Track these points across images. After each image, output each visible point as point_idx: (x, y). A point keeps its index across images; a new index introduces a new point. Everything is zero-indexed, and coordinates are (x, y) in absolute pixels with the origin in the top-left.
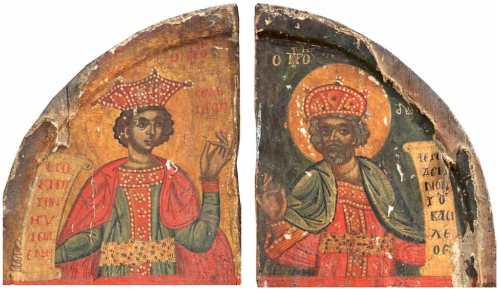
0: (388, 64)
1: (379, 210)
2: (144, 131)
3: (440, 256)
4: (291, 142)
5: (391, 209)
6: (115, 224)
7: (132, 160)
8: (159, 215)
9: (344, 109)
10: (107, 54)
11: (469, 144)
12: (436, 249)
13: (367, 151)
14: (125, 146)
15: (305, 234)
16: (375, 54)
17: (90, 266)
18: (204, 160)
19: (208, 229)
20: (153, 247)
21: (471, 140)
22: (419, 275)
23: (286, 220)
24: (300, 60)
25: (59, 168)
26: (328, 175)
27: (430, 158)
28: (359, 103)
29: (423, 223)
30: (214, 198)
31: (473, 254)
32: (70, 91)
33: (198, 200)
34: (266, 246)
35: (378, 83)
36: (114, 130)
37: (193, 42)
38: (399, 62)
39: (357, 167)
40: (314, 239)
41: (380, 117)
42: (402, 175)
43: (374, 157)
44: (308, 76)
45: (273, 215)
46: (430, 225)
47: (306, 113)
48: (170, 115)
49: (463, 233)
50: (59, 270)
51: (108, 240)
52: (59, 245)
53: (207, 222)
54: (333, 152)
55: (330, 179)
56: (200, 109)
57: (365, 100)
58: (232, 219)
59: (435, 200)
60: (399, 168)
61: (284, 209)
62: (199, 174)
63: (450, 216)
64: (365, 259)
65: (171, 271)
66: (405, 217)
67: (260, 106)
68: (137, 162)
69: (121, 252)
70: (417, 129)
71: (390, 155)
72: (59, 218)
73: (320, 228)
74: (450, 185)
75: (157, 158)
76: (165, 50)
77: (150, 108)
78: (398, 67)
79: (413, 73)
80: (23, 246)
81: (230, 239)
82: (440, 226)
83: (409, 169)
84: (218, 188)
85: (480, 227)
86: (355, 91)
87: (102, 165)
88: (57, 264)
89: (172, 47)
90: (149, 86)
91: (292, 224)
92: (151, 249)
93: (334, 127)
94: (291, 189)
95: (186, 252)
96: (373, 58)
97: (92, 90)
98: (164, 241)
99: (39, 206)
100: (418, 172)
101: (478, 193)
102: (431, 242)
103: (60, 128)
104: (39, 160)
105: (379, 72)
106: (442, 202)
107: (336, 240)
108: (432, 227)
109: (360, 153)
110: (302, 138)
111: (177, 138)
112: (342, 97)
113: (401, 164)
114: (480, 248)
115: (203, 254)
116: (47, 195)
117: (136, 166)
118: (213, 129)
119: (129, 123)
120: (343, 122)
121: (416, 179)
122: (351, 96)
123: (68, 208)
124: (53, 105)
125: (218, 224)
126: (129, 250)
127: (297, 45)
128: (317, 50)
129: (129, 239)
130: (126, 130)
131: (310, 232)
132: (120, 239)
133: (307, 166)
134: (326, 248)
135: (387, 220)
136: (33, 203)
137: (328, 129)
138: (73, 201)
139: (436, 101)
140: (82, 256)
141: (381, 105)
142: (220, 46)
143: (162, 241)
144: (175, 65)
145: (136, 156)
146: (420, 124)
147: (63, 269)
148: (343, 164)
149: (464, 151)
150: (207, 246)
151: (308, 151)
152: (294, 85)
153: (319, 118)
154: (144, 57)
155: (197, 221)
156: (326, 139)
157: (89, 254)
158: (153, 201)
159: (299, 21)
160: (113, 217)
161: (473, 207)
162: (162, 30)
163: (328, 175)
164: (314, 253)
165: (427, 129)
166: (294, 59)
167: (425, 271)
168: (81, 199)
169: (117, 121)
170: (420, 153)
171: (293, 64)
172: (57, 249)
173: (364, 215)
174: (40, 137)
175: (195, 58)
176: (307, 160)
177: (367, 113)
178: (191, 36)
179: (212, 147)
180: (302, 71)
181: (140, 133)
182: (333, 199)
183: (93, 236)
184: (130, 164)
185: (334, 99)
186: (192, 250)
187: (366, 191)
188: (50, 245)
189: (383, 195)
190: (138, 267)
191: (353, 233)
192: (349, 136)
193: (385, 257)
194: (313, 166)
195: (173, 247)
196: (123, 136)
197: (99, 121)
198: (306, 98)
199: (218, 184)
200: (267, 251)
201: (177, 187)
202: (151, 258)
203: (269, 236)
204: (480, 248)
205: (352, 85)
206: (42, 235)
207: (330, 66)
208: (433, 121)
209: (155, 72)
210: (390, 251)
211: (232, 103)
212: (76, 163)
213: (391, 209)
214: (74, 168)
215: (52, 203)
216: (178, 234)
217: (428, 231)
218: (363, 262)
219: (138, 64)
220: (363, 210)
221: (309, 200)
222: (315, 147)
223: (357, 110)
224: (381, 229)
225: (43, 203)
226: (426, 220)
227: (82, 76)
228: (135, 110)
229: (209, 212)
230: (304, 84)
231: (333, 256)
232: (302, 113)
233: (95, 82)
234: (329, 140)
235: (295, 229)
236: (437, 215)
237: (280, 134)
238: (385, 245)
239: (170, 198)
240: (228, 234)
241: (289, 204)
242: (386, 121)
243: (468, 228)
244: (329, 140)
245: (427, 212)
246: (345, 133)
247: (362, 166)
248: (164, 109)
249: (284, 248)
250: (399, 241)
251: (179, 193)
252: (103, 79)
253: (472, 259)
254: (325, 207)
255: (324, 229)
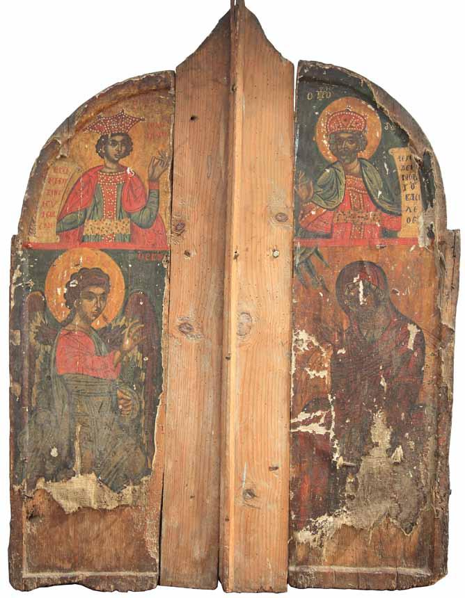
0: (381, 96)
1: (372, 193)
2: (114, 149)
3: (411, 224)
4: (317, 149)
5: (380, 193)
6: (94, 209)
7: (106, 167)
8: (121, 204)
9: (351, 127)
10: (94, 98)
11: (431, 148)
12: (409, 220)
13: (365, 154)
14: (102, 157)
15: (324, 210)
16: (373, 90)
17: (77, 235)
18: (151, 169)
19: (151, 214)
20: (117, 224)
21: (432, 146)
22: (397, 237)
23: (312, 202)
24: (325, 96)
25: (62, 170)
26: (340, 171)
27: (405, 159)
28: (361, 122)
29: (401, 203)
30: (156, 193)
31: (432, 223)
32: (69, 122)
33: (146, 195)
34: (299, 219)
35: (373, 109)
36: (96, 146)
37: (147, 92)
38: (388, 95)
39: (359, 165)
40: (330, 214)
41: (374, 131)
42: (387, 170)
43: (370, 159)
44: (329, 106)
45: (304, 198)
46: (405, 203)
47: (327, 130)
48: (131, 139)
49: (426, 209)
50: (58, 237)
51: (89, 219)
52: (59, 220)
53: (150, 209)
54: (344, 155)
55: (341, 174)
56: (150, 136)
57: (365, 121)
58: (166, 208)
59: (408, 187)
60: (386, 165)
61: (311, 195)
62: (147, 178)
63: (418, 198)
64: (363, 227)
65: (127, 240)
66: (389, 199)
67: (298, 127)
68: (109, 168)
69: (96, 226)
70: (397, 140)
71: (380, 157)
72: (59, 203)
73: (334, 207)
74: (418, 177)
75: (122, 166)
76: (130, 97)
77: (118, 134)
78: (387, 97)
79: (396, 102)
80: (37, 221)
81: (164, 220)
82: (411, 204)
83: (392, 166)
84: (159, 187)
85: (437, 204)
86: (359, 115)
87: (88, 169)
88: (58, 233)
89: (133, 96)
90: (118, 120)
91: (317, 205)
92: (115, 225)
93: (344, 139)
94: (316, 181)
95: (137, 228)
96: (371, 92)
97: (83, 120)
98: (124, 220)
99: (48, 194)
100: (398, 168)
101: (436, 181)
102: (405, 215)
103: (63, 146)
104: (49, 165)
105: (375, 102)
106: (413, 187)
107: (344, 215)
108: (406, 205)
109: (361, 155)
110: (324, 148)
111: (135, 154)
112: (350, 119)
113: (387, 163)
114: (437, 218)
115: (147, 230)
116: (53, 188)
117: (108, 171)
118: (157, 149)
119: (106, 143)
120: (351, 135)
121: (397, 172)
122: (356, 118)
123: (66, 197)
124: (59, 130)
125: (158, 211)
126: (102, 225)
127: (323, 86)
128: (335, 89)
129: (102, 218)
130: (103, 147)
131: (327, 209)
132: (97, 218)
133: (327, 165)
134: (338, 220)
135: (377, 201)
136: (45, 193)
137: (340, 140)
138: (69, 192)
139: (411, 120)
140: (73, 228)
141: (375, 124)
142: (163, 96)
143: (122, 221)
144: (135, 107)
145: (109, 165)
146: (400, 136)
147: (60, 236)
148: (350, 163)
149: (428, 153)
150: (150, 224)
151: (328, 155)
152: (320, 112)
153: (335, 133)
154: (116, 101)
155: (145, 208)
156: (339, 147)
157: (77, 227)
158: (117, 194)
159: (326, 70)
160: (93, 203)
161: (432, 190)
162: (129, 83)
163: (340, 171)
164: (330, 223)
165: (404, 138)
166: (321, 95)
167: (401, 235)
168: (73, 192)
169: (98, 141)
170: (400, 155)
171: (320, 98)
172: (57, 223)
173: (363, 198)
174: (50, 149)
175: (148, 103)
176: (327, 161)
177: (366, 129)
178: (145, 88)
179: (156, 161)
180: (326, 103)
181: (112, 150)
182: (343, 187)
183: (80, 215)
184: (105, 170)
185: (345, 120)
186: (141, 226)
187: (364, 181)
188: (53, 220)
189: (375, 183)
190: (106, 237)
191: (355, 209)
192: (354, 145)
193: (376, 225)
194: (330, 166)
195: (129, 225)
196: (101, 152)
197: (87, 141)
198: (328, 120)
199: (159, 184)
200: (300, 222)
201: (133, 185)
202: (115, 231)
203: (302, 212)
204: (437, 218)
205: (357, 111)
206: (49, 214)
207: (344, 99)
208: (408, 133)
209: (123, 111)
210: (379, 221)
211: (169, 133)
212: (73, 168)
213: (380, 193)
214: (70, 170)
215: (56, 192)
216: (133, 216)
217: (404, 209)
218: (361, 229)
219: (112, 105)
220: (362, 193)
221: (328, 187)
222: (332, 152)
223: (360, 127)
224: (374, 207)
225: (51, 193)
226: (403, 200)
227: (78, 112)
228: (110, 135)
229: (153, 202)
230: (327, 111)
231: (342, 225)
232: (325, 130)
233: (85, 116)
234: (342, 148)
235: (318, 207)
236: (409, 197)
237: (310, 144)
238: (376, 217)
239: (128, 192)
240: (163, 216)
241: (315, 191)
242: (378, 135)
243: (429, 205)
244: (342, 148)
245: (403, 195)
246: (352, 142)
247: (362, 165)
248: (128, 135)
249: (311, 220)
250: (384, 214)
251: (134, 189)
252: (91, 113)
253: (432, 225)
254: (338, 192)
255: (337, 207)
